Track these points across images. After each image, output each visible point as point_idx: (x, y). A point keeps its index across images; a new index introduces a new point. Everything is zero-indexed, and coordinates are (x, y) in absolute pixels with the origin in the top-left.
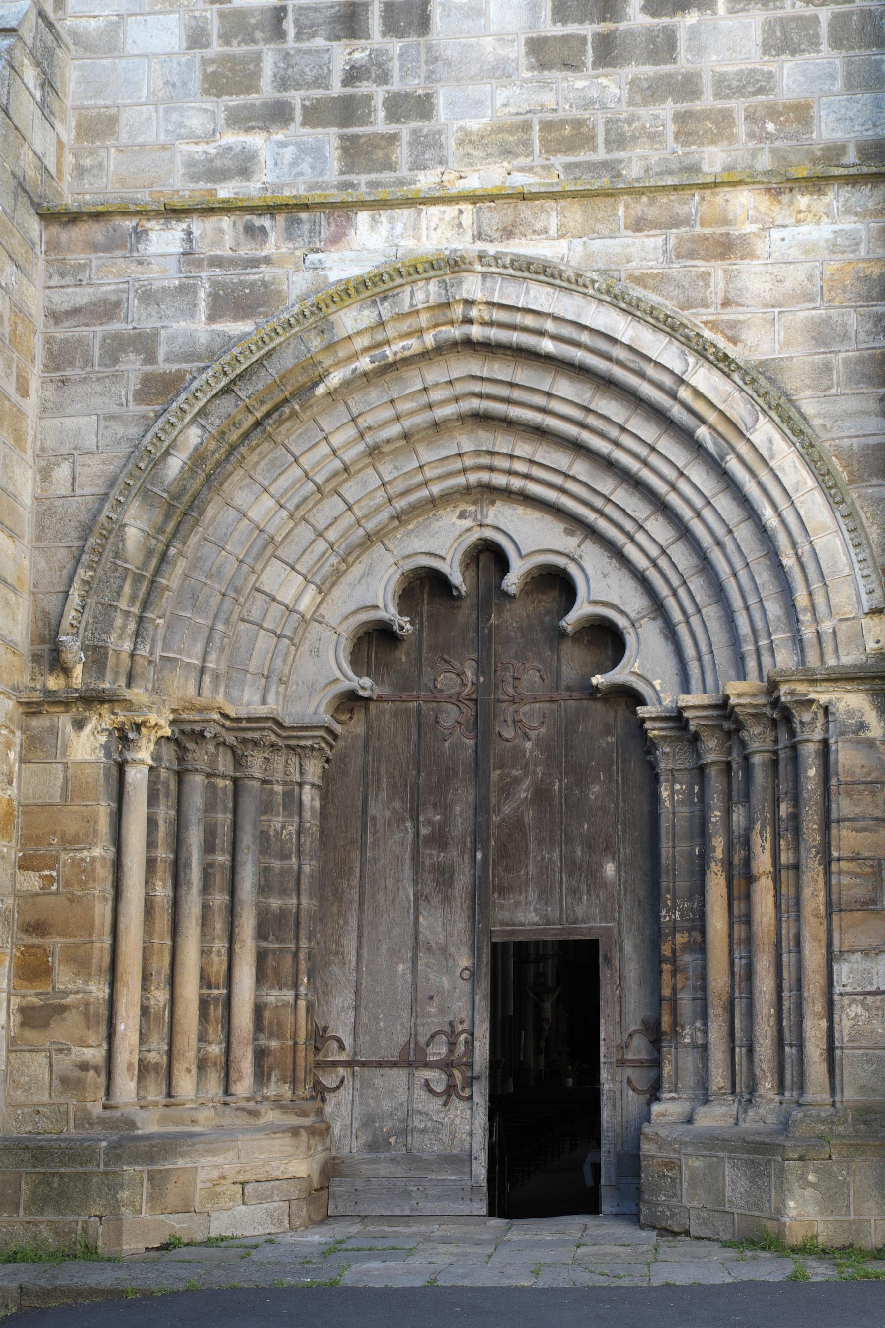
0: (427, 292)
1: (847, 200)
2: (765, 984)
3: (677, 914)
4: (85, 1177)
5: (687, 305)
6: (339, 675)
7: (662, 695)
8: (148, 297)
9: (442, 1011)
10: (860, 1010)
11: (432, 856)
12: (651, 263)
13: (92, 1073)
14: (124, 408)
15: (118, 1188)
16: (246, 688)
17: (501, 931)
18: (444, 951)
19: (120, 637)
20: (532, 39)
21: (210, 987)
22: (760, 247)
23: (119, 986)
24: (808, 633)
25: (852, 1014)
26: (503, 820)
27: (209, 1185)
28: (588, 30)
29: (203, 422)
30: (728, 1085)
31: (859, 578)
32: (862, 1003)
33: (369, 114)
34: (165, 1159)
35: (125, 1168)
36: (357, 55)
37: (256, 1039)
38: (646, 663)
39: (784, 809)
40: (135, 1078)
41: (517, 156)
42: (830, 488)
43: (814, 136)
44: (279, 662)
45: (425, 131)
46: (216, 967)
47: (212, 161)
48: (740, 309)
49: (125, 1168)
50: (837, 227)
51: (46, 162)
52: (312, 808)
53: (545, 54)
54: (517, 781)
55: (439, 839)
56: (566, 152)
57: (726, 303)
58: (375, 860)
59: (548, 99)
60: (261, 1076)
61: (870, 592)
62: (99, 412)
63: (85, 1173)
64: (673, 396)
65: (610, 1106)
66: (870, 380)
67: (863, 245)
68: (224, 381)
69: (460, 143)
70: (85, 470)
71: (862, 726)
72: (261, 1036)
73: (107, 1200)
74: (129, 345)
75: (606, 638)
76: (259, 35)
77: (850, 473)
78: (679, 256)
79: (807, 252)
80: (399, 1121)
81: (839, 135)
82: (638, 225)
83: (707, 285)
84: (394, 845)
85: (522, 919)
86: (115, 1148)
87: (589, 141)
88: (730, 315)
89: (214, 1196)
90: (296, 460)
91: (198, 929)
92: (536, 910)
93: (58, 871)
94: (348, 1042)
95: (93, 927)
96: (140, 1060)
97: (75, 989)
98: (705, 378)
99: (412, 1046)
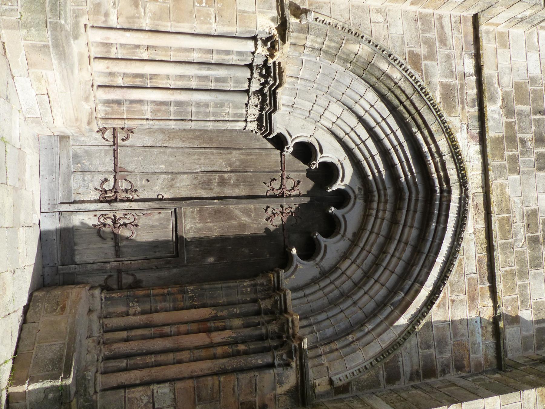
1: (491, 347)
2: (159, 344)
3: (191, 295)
4: (44, 10)
5: (451, 285)
6: (293, 138)
7: (288, 279)
8: (448, 58)
9: (143, 186)
10: (145, 401)
11: (216, 178)
12: (466, 268)
13: (103, 19)
14: (406, 46)
15: (37, 28)
16: (288, 97)
17: (181, 212)
18: (172, 186)
19: (312, 40)
20: (536, 211)
21: (150, 79)
23: (150, 34)
24: (321, 350)
25: (143, 398)
26: (232, 211)
27: (45, 77)
29: (402, 79)
30: (108, 329)
31: (346, 373)
32: (149, 402)
33: (510, 148)
34: (56, 54)
35: (49, 32)
36: (529, 143)
37: (126, 100)
38: (302, 270)
39: (242, 347)
40: (102, 41)
41: (498, 208)
42: (383, 356)
43: (507, 326)
44: (299, 111)
45: (505, 171)
46: (160, 81)
47: (492, 85)
48: (450, 307)
49: (49, 32)
50: (481, 344)
51: (495, 18)
52: (235, 126)
54: (249, 215)
55: (222, 183)
56: (500, 227)
57: (453, 301)
58: (213, 154)
59: (517, 219)
60: (108, 102)
61: (340, 380)
62: (405, 35)
63: (46, 11)
64: (415, 281)
65: (98, 268)
66: (425, 366)
67: (474, 355)
68: (419, 89)
69: (501, 185)
70: (382, 28)
71: (281, 384)
72: (128, 103)
73: (30, 22)
74: (430, 49)
75: (310, 251)
76: (535, 105)
77: (388, 363)
78: (469, 279)
79: (472, 333)
80: (89, 168)
83: (459, 292)
84: (220, 162)
85: (188, 221)
86: (60, 28)
88: (448, 303)
89: (39, 79)
91: (179, 74)
92: (191, 227)
93: (205, 7)
94: (126, 143)
95: (178, 22)
96: (112, 44)
97: (146, 12)
99: (126, 173)
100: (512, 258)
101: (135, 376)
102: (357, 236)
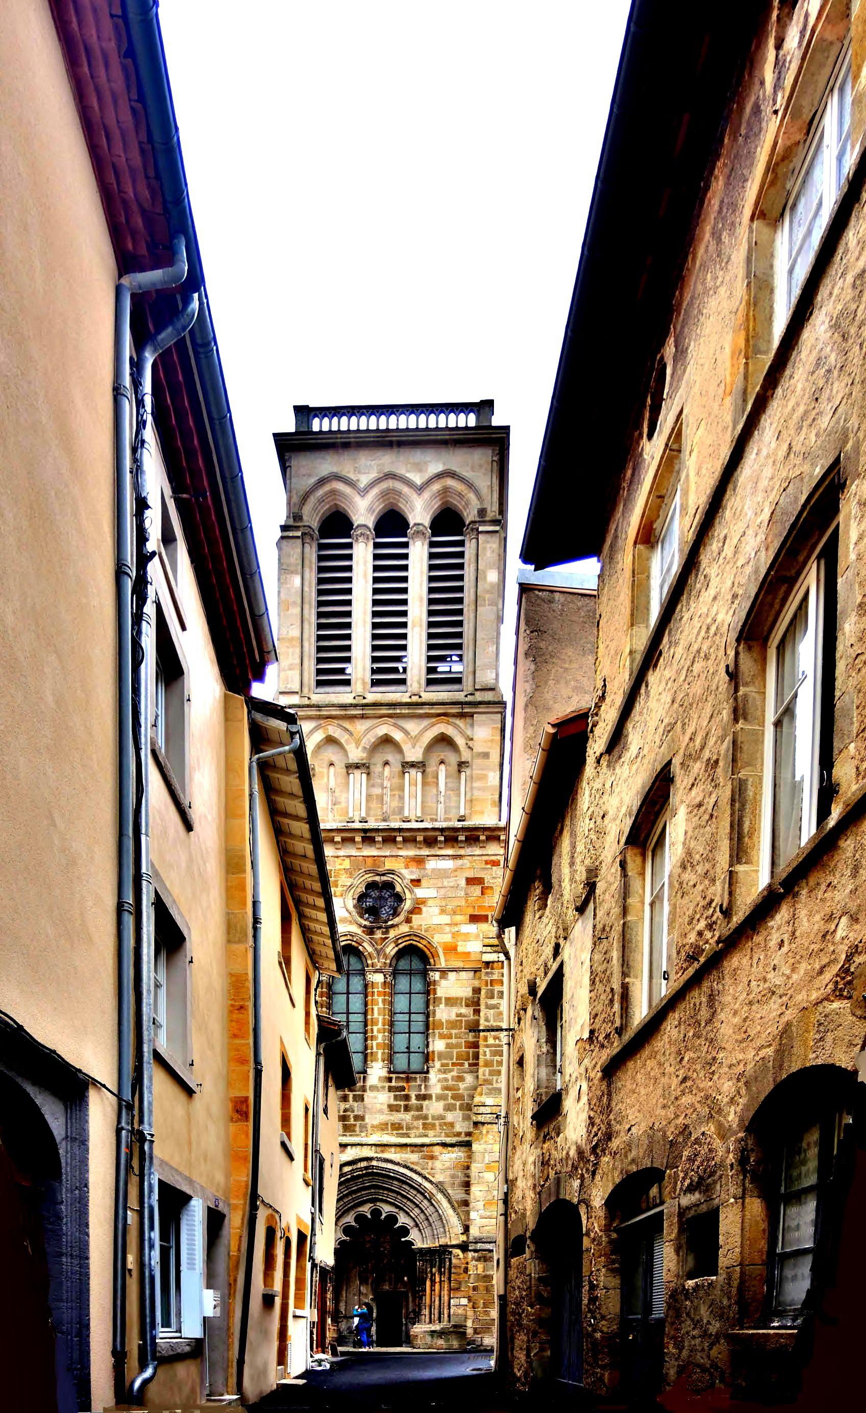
0: (363, 1164)
22: (440, 1158)
28: (402, 1103)
53: (392, 1108)
59: (392, 1118)
81: (460, 1130)
82: (412, 1152)
87: (402, 1128)
90: (348, 993)
98: (427, 1184)
100: (415, 1123)
101: (446, 1312)
102: (397, 1207)
